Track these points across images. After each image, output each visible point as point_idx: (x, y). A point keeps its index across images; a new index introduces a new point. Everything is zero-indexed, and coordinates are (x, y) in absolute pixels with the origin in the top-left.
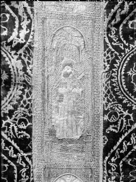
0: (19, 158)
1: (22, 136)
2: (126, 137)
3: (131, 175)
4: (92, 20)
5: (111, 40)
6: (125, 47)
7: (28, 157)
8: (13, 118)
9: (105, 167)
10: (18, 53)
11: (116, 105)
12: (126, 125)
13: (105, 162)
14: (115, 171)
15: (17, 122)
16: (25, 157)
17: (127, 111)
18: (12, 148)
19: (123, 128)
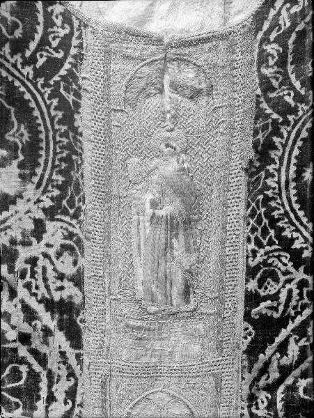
4: (214, 376)
8: (43, 242)
11: (276, 254)
12: (298, 301)
17: (302, 269)
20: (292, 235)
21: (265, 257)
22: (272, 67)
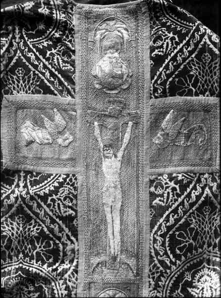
1: (66, 68)
2: (173, 57)
5: (157, 254)
6: (171, 262)
17: (171, 33)
18: (57, 226)
19: (169, 49)
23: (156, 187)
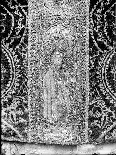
0: (16, 9)
3: (113, 24)
5: (96, 35)
7: (24, 9)
9: (91, 18)
10: (15, 49)
11: (100, 101)
12: (108, 122)
13: (92, 13)
14: (100, 20)
15: (15, 109)
16: (22, 8)
20: (106, 94)
21: (96, 102)
22: (98, 29)
23: (94, 112)
